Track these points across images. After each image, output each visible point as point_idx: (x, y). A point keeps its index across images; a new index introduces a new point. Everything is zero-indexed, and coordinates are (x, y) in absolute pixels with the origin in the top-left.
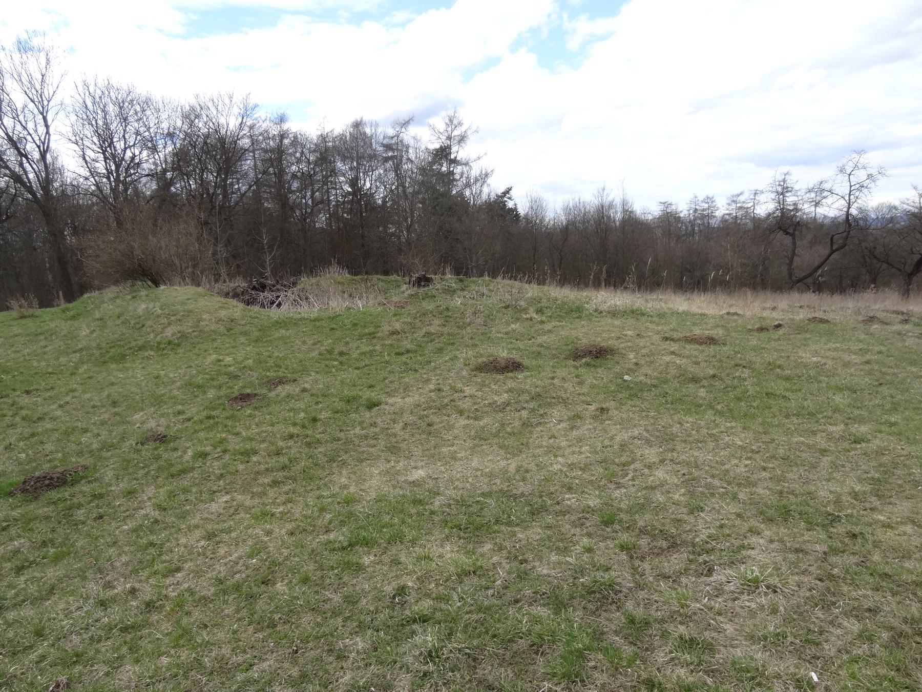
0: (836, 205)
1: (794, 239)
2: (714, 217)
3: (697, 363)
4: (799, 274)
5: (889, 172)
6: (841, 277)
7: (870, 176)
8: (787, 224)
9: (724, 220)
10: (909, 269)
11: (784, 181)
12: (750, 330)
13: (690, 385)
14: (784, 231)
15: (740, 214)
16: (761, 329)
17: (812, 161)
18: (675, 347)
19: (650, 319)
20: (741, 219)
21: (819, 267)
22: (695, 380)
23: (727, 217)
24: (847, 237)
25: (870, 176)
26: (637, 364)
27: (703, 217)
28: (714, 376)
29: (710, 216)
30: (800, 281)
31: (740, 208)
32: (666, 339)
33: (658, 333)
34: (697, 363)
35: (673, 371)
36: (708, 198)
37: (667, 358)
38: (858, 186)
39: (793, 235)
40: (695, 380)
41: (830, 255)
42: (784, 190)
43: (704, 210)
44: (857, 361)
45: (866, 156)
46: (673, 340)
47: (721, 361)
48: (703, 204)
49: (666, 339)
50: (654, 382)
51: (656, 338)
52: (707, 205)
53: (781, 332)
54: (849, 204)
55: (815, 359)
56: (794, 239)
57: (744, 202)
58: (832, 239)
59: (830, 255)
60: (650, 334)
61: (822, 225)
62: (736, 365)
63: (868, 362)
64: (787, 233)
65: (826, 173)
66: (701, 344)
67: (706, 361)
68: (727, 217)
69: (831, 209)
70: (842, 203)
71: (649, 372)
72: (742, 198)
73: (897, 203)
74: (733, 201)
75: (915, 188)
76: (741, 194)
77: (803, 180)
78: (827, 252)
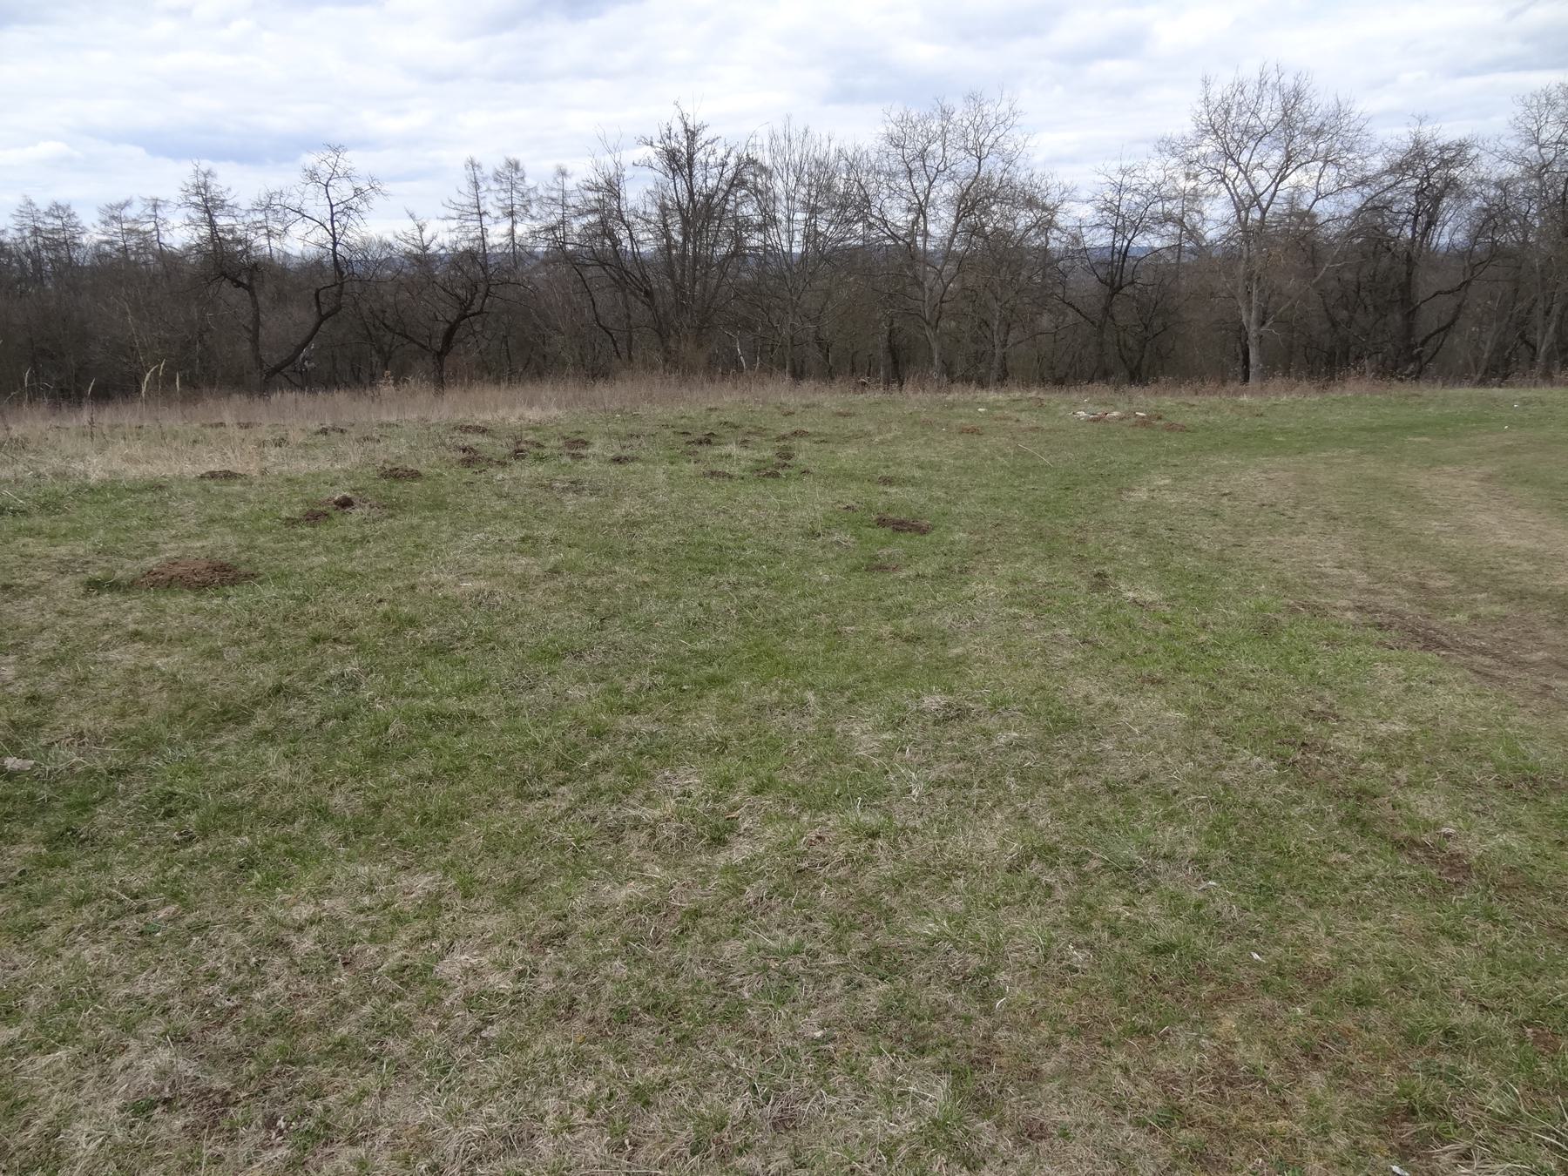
0: (312, 238)
1: (252, 294)
2: (79, 246)
3: (214, 654)
4: (272, 358)
5: (385, 188)
6: (334, 358)
7: (358, 192)
8: (227, 268)
9: (100, 255)
10: (438, 344)
11: (206, 186)
12: (291, 522)
13: (225, 737)
14: (233, 280)
15: (133, 241)
16: (314, 517)
17: (247, 155)
18: (133, 611)
19: (24, 523)
20: (136, 253)
21: (305, 344)
22: (231, 715)
23: (107, 248)
24: (340, 294)
25: (358, 192)
26: (33, 699)
27: (55, 245)
28: (278, 690)
29: (70, 244)
30: (277, 370)
31: (130, 231)
32: (95, 586)
33: (64, 567)
34: (214, 654)
35: (159, 700)
36: (58, 207)
37: (124, 656)
38: (342, 206)
39: (249, 288)
40: (231, 715)
41: (318, 325)
42: (209, 206)
43: (53, 231)
44: (536, 571)
45: (347, 155)
46: (115, 586)
47: (270, 634)
48: (49, 220)
49: (95, 586)
50: (114, 756)
51: (67, 586)
52: (58, 222)
53: (356, 514)
54: (334, 236)
55: (468, 585)
56: (252, 294)
57: (135, 221)
58: (317, 296)
59: (318, 325)
60: (42, 575)
61: (284, 270)
62: (316, 640)
63: (555, 571)
64: (239, 284)
65: (284, 180)
66: (201, 587)
67: (237, 643)
68: (107, 248)
69: (299, 242)
70: (322, 235)
71: (86, 723)
72: (130, 213)
73: (389, 238)
74: (113, 217)
75: (412, 216)
76: (127, 204)
77: (242, 189)
78: (310, 319)
